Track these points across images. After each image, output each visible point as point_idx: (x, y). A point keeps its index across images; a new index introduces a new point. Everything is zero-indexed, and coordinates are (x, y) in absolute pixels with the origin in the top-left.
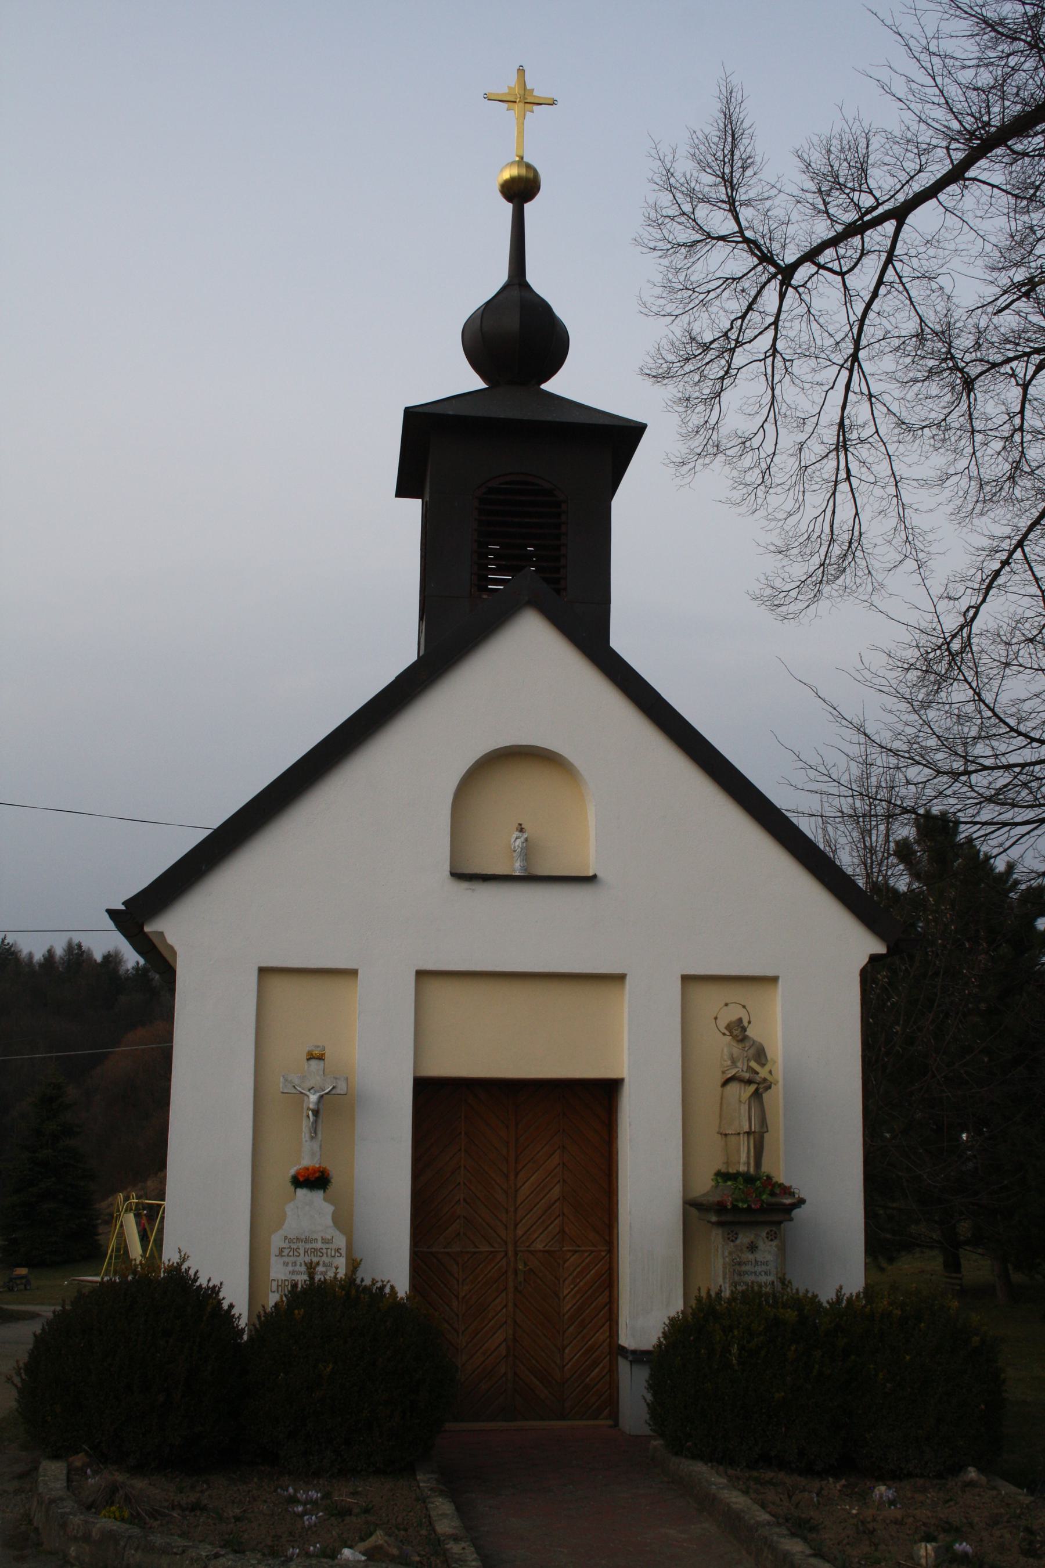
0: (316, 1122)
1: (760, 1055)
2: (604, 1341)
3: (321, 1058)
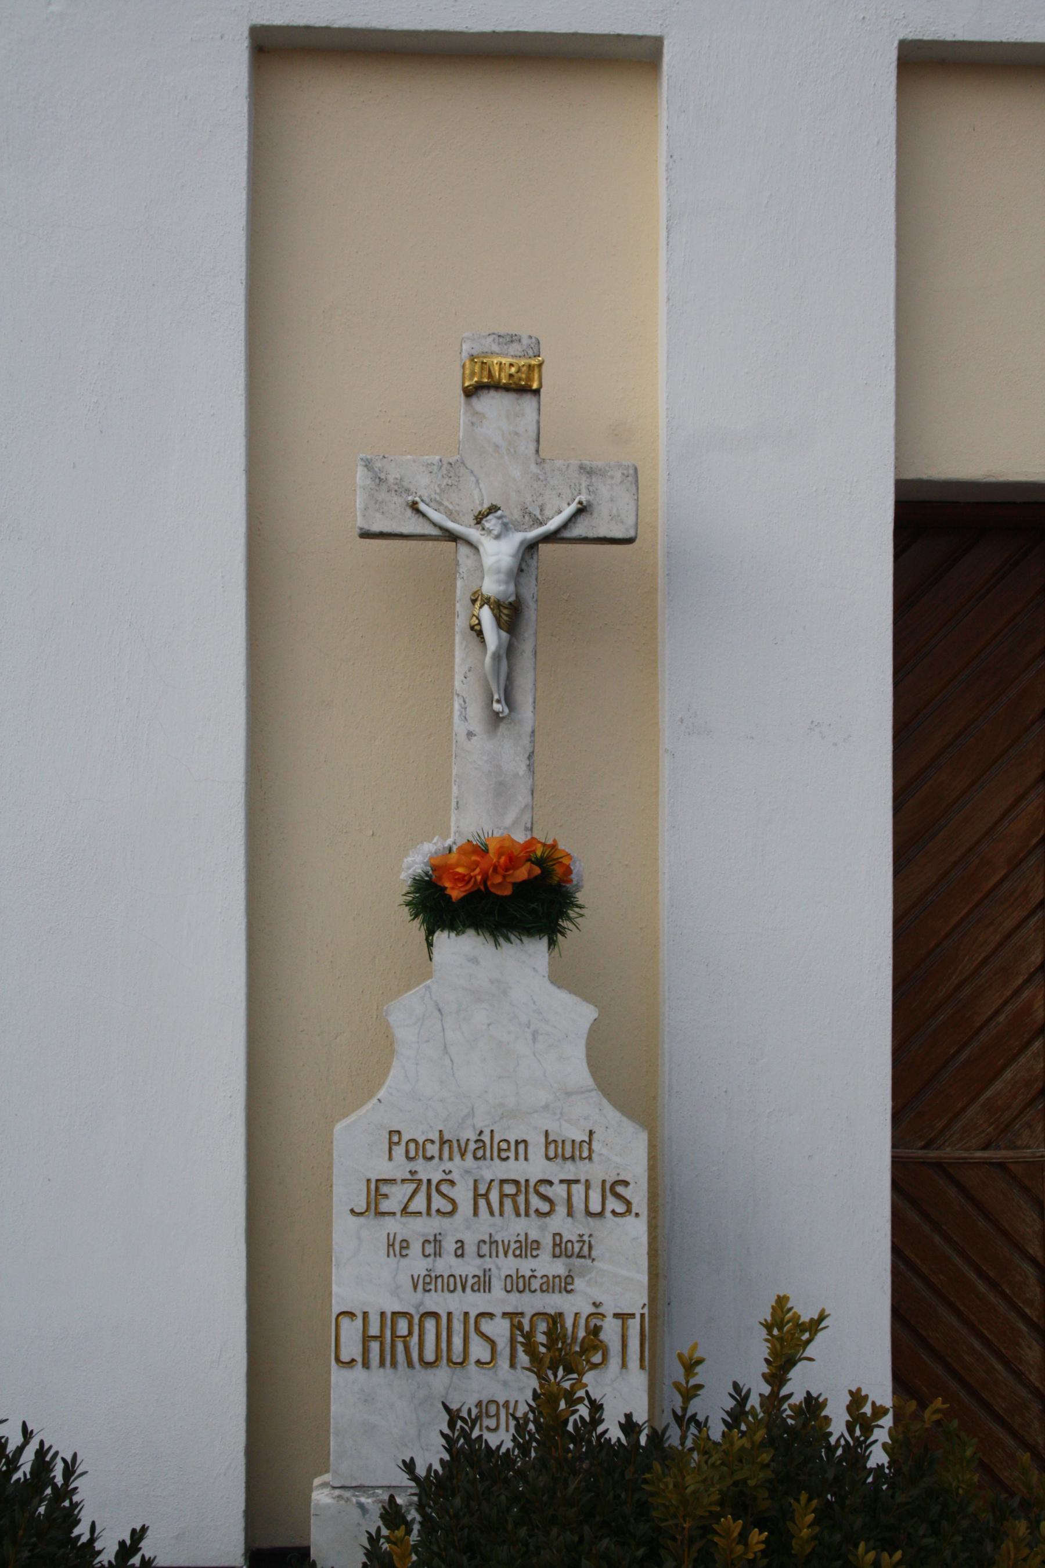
0: (509, 652)
3: (522, 387)
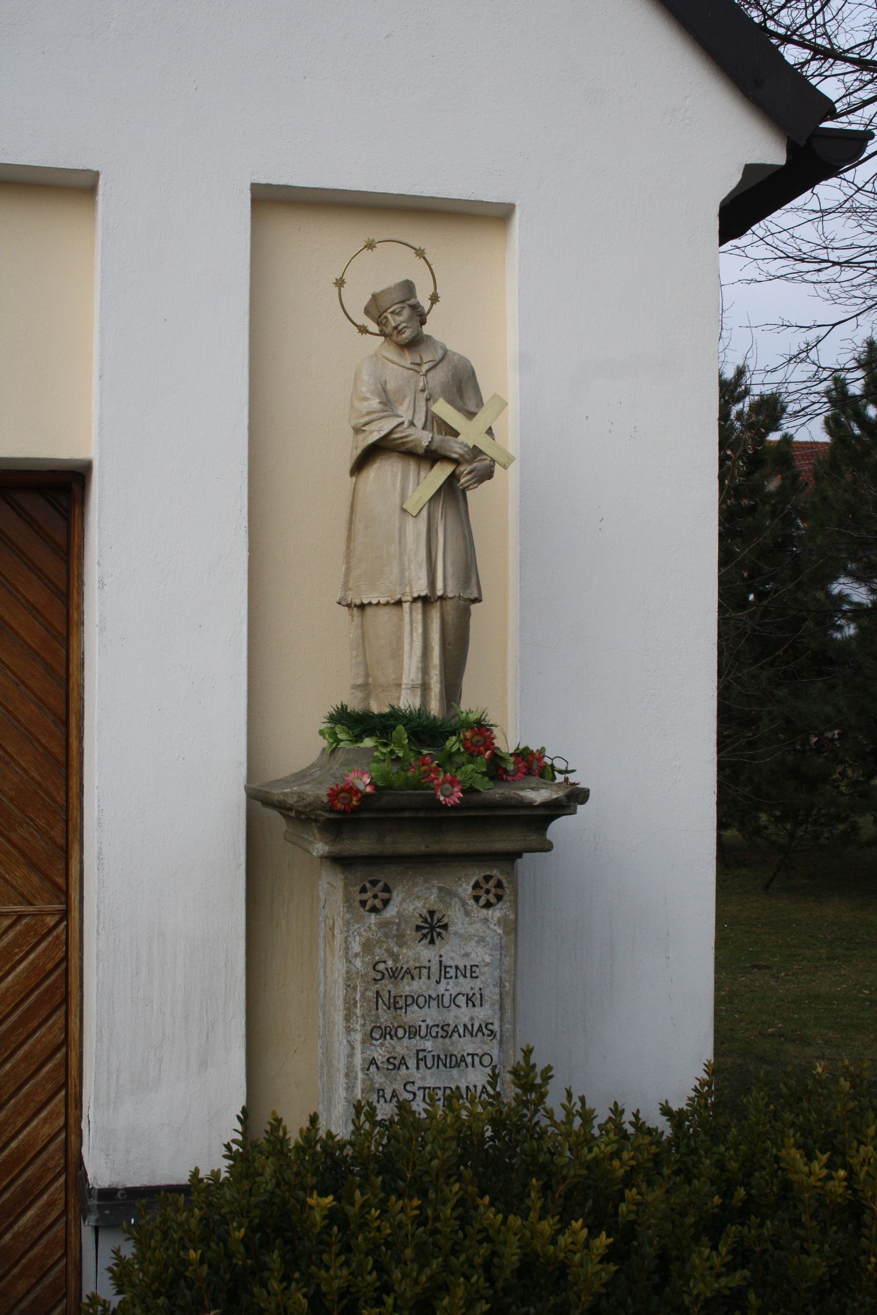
1: (463, 387)
2: (52, 1139)
